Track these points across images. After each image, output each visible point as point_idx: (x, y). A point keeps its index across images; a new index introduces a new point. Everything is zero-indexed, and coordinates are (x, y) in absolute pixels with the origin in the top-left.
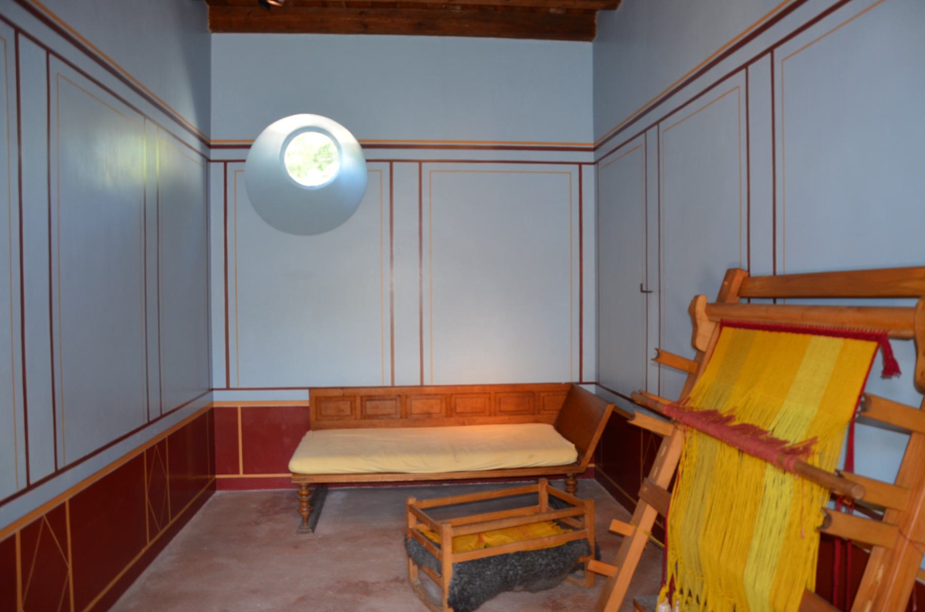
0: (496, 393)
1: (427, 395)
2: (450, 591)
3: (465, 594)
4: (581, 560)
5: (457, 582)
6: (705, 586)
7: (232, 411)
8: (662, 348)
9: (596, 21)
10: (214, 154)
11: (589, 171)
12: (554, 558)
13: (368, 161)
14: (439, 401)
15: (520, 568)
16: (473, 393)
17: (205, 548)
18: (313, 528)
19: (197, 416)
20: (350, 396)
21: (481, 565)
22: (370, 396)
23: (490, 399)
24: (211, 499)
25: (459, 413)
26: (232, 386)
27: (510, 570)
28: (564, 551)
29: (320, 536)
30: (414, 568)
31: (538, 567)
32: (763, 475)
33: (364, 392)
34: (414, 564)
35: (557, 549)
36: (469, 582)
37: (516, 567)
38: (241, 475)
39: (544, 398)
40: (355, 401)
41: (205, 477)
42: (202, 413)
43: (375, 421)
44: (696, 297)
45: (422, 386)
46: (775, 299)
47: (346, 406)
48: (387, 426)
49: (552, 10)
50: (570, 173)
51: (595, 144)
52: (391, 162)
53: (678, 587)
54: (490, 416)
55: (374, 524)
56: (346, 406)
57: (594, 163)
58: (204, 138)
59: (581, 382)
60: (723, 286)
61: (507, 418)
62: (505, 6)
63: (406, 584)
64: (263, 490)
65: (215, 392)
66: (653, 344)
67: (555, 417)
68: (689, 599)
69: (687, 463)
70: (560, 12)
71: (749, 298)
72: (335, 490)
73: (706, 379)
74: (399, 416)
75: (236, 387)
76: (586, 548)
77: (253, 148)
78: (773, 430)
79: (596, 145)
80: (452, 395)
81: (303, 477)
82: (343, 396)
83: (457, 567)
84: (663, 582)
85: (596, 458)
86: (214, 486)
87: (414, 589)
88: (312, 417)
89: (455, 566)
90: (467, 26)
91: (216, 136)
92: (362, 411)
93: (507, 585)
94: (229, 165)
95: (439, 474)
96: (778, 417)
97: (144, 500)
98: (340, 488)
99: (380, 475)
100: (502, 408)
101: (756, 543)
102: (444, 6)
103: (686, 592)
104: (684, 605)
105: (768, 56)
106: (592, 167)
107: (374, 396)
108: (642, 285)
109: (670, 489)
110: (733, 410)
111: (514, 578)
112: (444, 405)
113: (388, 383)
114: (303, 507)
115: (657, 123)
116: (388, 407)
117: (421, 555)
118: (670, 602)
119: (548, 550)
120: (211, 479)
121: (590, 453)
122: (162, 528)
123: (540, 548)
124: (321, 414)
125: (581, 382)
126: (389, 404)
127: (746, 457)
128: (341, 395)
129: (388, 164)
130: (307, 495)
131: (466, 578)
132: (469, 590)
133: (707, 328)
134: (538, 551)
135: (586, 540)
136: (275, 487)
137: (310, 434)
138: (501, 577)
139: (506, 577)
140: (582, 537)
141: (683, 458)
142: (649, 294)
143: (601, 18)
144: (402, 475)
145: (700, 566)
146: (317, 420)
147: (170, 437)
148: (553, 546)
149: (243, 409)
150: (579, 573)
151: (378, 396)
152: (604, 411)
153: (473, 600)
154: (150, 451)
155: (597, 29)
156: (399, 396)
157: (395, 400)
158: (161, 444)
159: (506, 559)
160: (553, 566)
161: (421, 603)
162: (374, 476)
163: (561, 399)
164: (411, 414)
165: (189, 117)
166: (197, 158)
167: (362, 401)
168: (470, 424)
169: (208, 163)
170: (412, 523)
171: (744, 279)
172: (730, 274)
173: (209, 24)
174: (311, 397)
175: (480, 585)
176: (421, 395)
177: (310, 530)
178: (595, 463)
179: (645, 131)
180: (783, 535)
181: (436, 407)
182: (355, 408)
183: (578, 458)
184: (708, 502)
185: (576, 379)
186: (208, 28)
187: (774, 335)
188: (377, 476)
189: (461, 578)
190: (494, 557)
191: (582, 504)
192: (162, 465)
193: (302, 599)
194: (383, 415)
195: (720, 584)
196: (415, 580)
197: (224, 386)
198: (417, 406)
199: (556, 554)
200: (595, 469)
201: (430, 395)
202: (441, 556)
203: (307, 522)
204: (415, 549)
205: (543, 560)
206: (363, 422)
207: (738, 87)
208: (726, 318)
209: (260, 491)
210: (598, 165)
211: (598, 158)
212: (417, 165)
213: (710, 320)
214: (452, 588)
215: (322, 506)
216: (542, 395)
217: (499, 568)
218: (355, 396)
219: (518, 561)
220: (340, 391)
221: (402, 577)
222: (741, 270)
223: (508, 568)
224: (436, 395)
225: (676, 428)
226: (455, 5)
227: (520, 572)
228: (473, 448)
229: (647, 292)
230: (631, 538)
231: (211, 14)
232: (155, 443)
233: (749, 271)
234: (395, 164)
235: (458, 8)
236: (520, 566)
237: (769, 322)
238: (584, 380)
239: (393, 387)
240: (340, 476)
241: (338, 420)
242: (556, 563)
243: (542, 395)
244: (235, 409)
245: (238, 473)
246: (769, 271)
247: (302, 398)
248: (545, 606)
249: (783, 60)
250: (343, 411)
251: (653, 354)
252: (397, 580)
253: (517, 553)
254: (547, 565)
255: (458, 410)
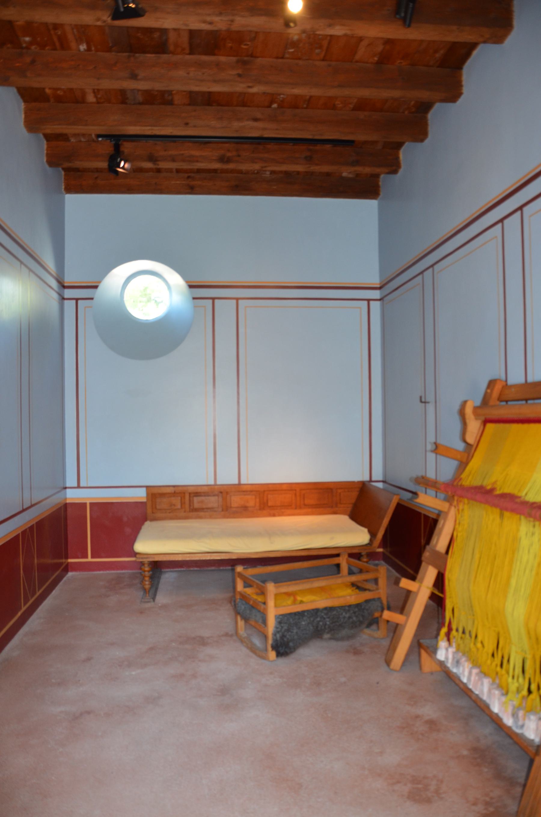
0: (301, 490)
1: (244, 491)
2: (273, 637)
3: (285, 639)
4: (377, 615)
5: (279, 630)
6: (476, 622)
7: (83, 506)
8: (438, 442)
9: (380, 183)
10: (68, 293)
11: (376, 306)
12: (355, 613)
13: (194, 298)
14: (254, 497)
15: (327, 620)
16: (282, 490)
17: (67, 614)
18: (154, 599)
19: (54, 509)
20: (180, 493)
21: (297, 617)
22: (197, 493)
23: (296, 495)
24: (65, 579)
25: (270, 507)
26: (82, 485)
27: (320, 621)
28: (363, 607)
29: (160, 605)
30: (241, 623)
31: (342, 620)
32: (518, 530)
33: (191, 490)
34: (241, 620)
35: (358, 605)
36: (288, 630)
37: (324, 618)
38: (90, 559)
39: (340, 494)
40: (184, 497)
41: (61, 561)
42: (59, 506)
43: (201, 514)
44: (465, 402)
45: (239, 484)
46: (526, 400)
47: (177, 501)
48: (211, 517)
49: (345, 174)
50: (360, 308)
51: (380, 284)
52: (213, 299)
53: (454, 627)
54: (296, 508)
55: (203, 596)
56: (177, 501)
57: (380, 300)
58: (60, 280)
59: (371, 481)
60: (486, 393)
61: (310, 510)
62: (306, 172)
63: (235, 638)
64: (108, 572)
65: (68, 490)
66: (431, 439)
67: (349, 509)
68: (463, 636)
69: (460, 529)
70: (351, 176)
71: (507, 401)
72: (167, 572)
73: (475, 464)
74: (220, 509)
75: (85, 485)
76: (380, 605)
77: (99, 288)
78: (526, 494)
79: (381, 285)
80: (264, 491)
81: (145, 556)
82: (175, 492)
83: (278, 618)
84: (443, 625)
85: (384, 543)
86: (67, 569)
87: (242, 641)
88: (149, 511)
89: (277, 617)
90: (275, 187)
91: (68, 279)
92: (190, 506)
93: (317, 634)
94: (79, 301)
95: (257, 553)
96: (529, 485)
97: (20, 574)
98: (172, 570)
99: (209, 554)
100: (307, 501)
101: (513, 582)
102: (256, 171)
103: (461, 630)
104: (459, 639)
105: (519, 213)
106: (378, 303)
107: (200, 493)
108: (421, 397)
109: (447, 552)
110: (495, 483)
111: (323, 628)
112: (258, 500)
113: (212, 482)
114: (145, 581)
115: (432, 266)
116: (213, 501)
117: (248, 612)
118: (449, 640)
119: (350, 606)
120: (65, 562)
121: (380, 535)
122: (32, 597)
123: (344, 605)
124: (156, 508)
125: (371, 481)
126: (213, 499)
127: (507, 514)
128: (173, 492)
129: (210, 301)
130: (149, 571)
131: (286, 627)
132: (288, 636)
133: (474, 426)
134: (342, 607)
135: (379, 599)
136: (118, 569)
137: (147, 524)
138: (313, 626)
139: (317, 627)
140: (376, 596)
141: (457, 526)
142: (427, 404)
143: (384, 180)
144: (227, 554)
145: (471, 607)
146: (153, 513)
147: (37, 523)
148: (354, 603)
149: (91, 504)
150: (374, 627)
151: (204, 493)
152: (391, 501)
153: (291, 644)
154: (24, 532)
155: (381, 189)
156: (221, 492)
157: (217, 495)
158: (31, 528)
159: (316, 613)
160: (354, 618)
161: (248, 651)
162: (204, 555)
163: (354, 494)
164: (231, 507)
165: (50, 263)
166: (55, 296)
167: (190, 496)
168: (279, 515)
169: (63, 300)
170: (240, 586)
171: (503, 387)
172: (492, 383)
173: (63, 187)
174: (148, 494)
175: (297, 633)
176: (239, 491)
177: (152, 600)
178: (383, 548)
179: (422, 273)
180: (534, 572)
181: (252, 501)
182: (185, 503)
183: (371, 540)
184: (477, 556)
185: (366, 478)
186: (63, 190)
187: (526, 426)
188: (207, 554)
189: (282, 627)
190: (308, 611)
191: (377, 570)
192: (32, 546)
193: (152, 649)
194: (207, 508)
195: (487, 618)
196: (242, 632)
197: (76, 485)
198: (236, 501)
199: (356, 610)
200: (383, 553)
201: (246, 491)
202: (266, 609)
203: (149, 594)
204: (243, 607)
205: (346, 613)
206: (191, 513)
207: (496, 237)
208: (488, 417)
209: (105, 572)
210: (383, 301)
211: (383, 296)
212: (235, 301)
213: (476, 419)
214: (274, 634)
215: (158, 582)
216: (339, 491)
217: (312, 619)
218: (184, 493)
219: (326, 614)
220: (172, 488)
221: (230, 633)
222: (500, 380)
223: (319, 619)
224: (251, 491)
225: (451, 505)
226: (266, 171)
227: (328, 623)
228: (284, 533)
229: (425, 402)
230: (417, 593)
231: (65, 179)
232: (27, 527)
233: (506, 381)
234: (216, 301)
235: (268, 173)
236: (328, 618)
237: (521, 417)
238: (373, 479)
239: (215, 485)
240: (176, 555)
241: (170, 513)
242: (357, 617)
243: (339, 491)
244: (85, 504)
245: (86, 557)
246: (522, 380)
247: (141, 495)
248: (347, 652)
249: (530, 216)
250: (174, 505)
251: (429, 447)
252: (226, 635)
253: (326, 609)
254: (350, 618)
255: (270, 504)
